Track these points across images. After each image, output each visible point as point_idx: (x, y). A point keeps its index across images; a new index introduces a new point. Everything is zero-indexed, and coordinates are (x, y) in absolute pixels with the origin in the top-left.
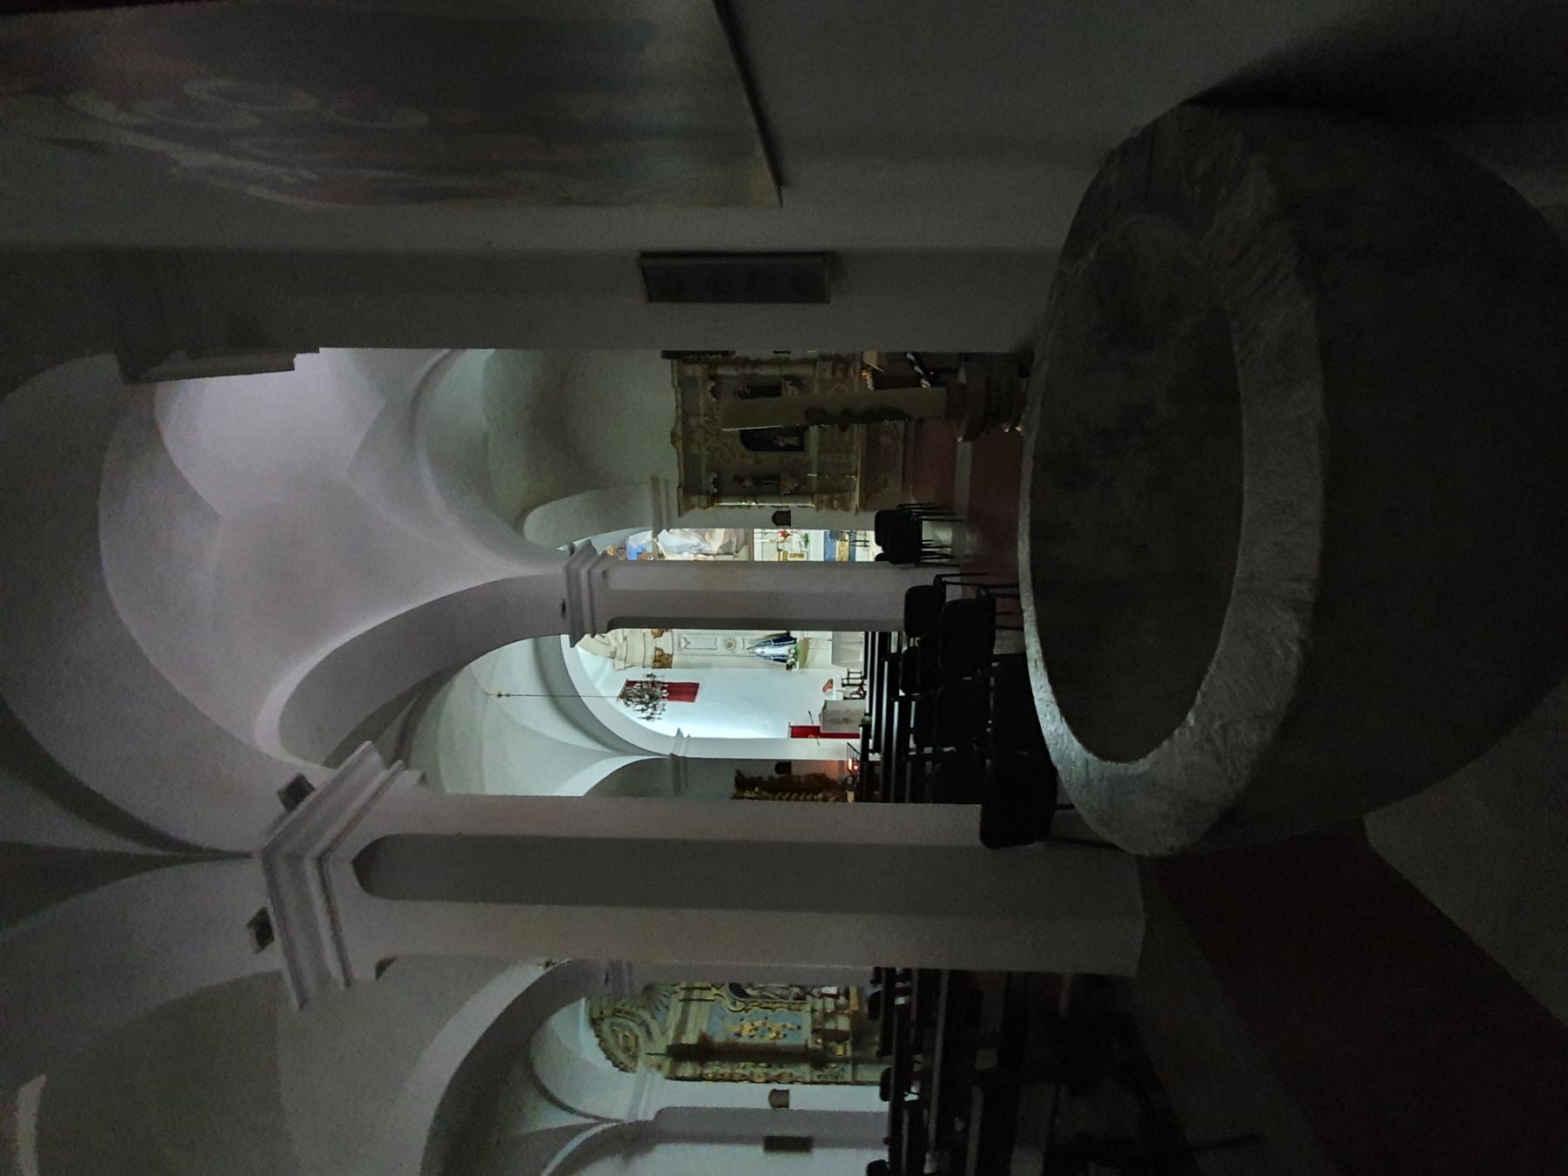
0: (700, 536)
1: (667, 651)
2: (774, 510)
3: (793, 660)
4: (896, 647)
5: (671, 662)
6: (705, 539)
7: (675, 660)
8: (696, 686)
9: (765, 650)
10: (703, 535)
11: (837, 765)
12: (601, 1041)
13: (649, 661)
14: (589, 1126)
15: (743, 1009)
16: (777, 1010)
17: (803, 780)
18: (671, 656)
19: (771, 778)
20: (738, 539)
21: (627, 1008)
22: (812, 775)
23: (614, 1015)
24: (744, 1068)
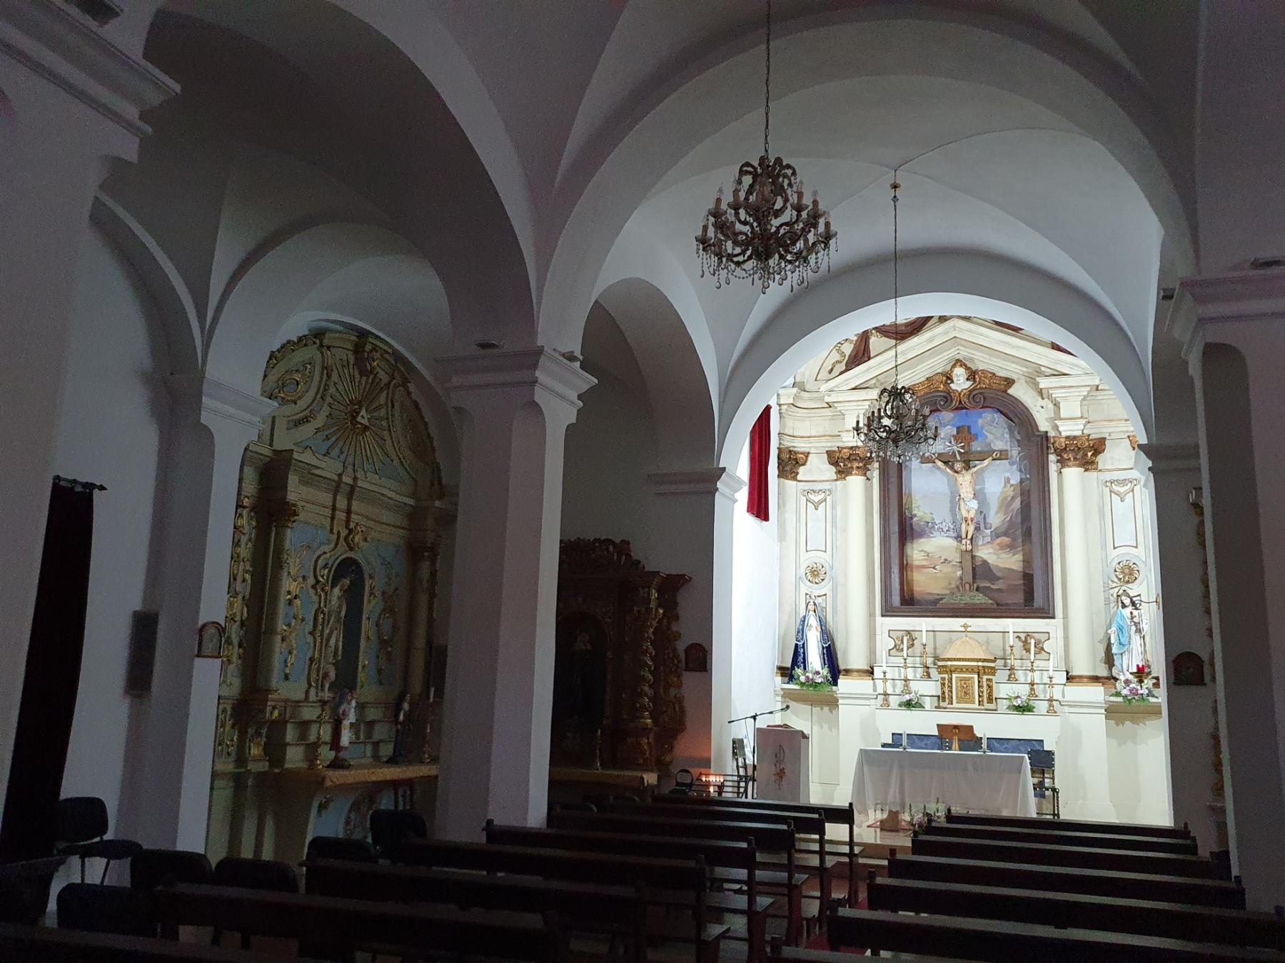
0: (1003, 529)
1: (803, 472)
2: (1205, 657)
3: (803, 679)
4: (883, 861)
5: (787, 478)
6: (998, 536)
7: (790, 484)
8: (766, 518)
9: (814, 629)
10: (1005, 534)
11: (705, 755)
12: (294, 343)
13: (787, 443)
14: (201, 318)
15: (318, 582)
16: (310, 639)
17: (673, 692)
18: (795, 479)
19: (678, 636)
20: (999, 590)
21: (332, 390)
22: (683, 711)
23: (324, 368)
24: (244, 581)
